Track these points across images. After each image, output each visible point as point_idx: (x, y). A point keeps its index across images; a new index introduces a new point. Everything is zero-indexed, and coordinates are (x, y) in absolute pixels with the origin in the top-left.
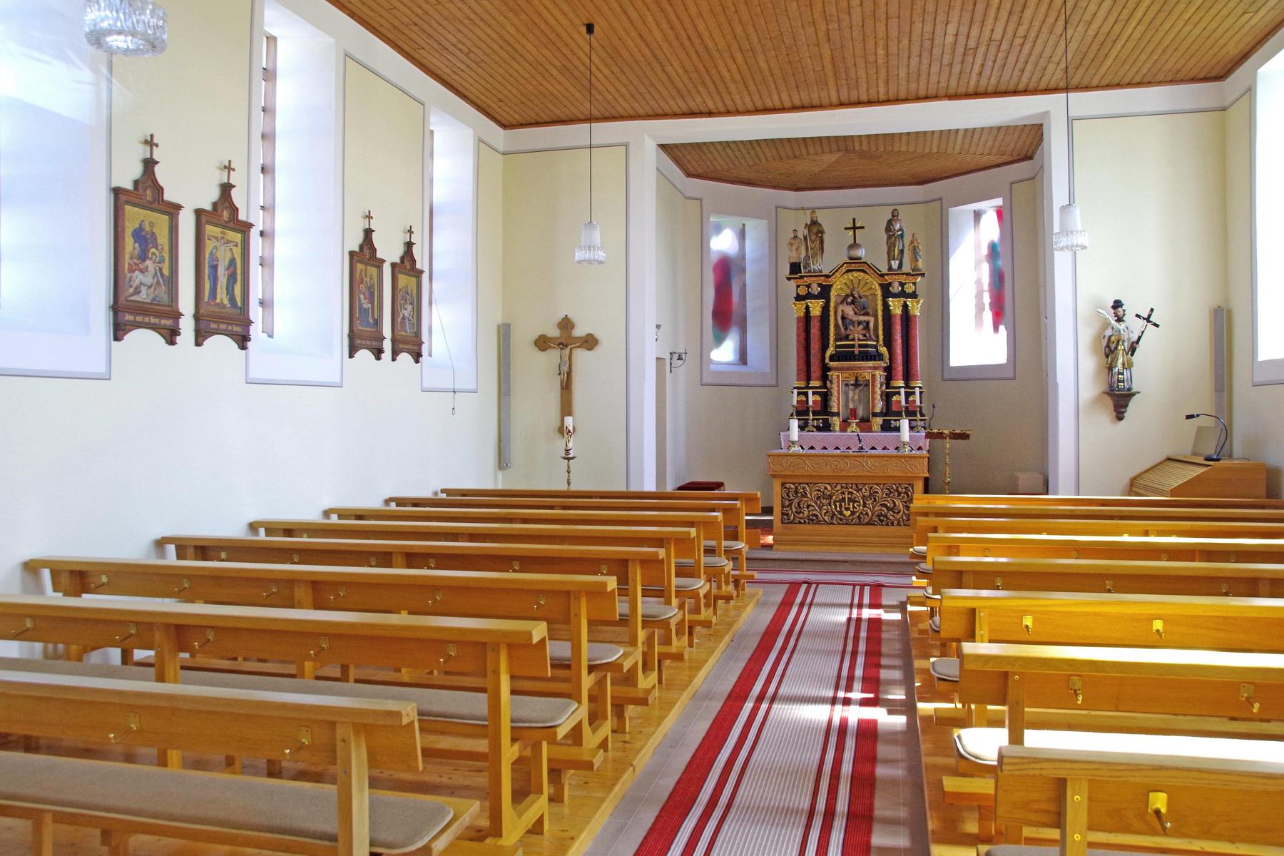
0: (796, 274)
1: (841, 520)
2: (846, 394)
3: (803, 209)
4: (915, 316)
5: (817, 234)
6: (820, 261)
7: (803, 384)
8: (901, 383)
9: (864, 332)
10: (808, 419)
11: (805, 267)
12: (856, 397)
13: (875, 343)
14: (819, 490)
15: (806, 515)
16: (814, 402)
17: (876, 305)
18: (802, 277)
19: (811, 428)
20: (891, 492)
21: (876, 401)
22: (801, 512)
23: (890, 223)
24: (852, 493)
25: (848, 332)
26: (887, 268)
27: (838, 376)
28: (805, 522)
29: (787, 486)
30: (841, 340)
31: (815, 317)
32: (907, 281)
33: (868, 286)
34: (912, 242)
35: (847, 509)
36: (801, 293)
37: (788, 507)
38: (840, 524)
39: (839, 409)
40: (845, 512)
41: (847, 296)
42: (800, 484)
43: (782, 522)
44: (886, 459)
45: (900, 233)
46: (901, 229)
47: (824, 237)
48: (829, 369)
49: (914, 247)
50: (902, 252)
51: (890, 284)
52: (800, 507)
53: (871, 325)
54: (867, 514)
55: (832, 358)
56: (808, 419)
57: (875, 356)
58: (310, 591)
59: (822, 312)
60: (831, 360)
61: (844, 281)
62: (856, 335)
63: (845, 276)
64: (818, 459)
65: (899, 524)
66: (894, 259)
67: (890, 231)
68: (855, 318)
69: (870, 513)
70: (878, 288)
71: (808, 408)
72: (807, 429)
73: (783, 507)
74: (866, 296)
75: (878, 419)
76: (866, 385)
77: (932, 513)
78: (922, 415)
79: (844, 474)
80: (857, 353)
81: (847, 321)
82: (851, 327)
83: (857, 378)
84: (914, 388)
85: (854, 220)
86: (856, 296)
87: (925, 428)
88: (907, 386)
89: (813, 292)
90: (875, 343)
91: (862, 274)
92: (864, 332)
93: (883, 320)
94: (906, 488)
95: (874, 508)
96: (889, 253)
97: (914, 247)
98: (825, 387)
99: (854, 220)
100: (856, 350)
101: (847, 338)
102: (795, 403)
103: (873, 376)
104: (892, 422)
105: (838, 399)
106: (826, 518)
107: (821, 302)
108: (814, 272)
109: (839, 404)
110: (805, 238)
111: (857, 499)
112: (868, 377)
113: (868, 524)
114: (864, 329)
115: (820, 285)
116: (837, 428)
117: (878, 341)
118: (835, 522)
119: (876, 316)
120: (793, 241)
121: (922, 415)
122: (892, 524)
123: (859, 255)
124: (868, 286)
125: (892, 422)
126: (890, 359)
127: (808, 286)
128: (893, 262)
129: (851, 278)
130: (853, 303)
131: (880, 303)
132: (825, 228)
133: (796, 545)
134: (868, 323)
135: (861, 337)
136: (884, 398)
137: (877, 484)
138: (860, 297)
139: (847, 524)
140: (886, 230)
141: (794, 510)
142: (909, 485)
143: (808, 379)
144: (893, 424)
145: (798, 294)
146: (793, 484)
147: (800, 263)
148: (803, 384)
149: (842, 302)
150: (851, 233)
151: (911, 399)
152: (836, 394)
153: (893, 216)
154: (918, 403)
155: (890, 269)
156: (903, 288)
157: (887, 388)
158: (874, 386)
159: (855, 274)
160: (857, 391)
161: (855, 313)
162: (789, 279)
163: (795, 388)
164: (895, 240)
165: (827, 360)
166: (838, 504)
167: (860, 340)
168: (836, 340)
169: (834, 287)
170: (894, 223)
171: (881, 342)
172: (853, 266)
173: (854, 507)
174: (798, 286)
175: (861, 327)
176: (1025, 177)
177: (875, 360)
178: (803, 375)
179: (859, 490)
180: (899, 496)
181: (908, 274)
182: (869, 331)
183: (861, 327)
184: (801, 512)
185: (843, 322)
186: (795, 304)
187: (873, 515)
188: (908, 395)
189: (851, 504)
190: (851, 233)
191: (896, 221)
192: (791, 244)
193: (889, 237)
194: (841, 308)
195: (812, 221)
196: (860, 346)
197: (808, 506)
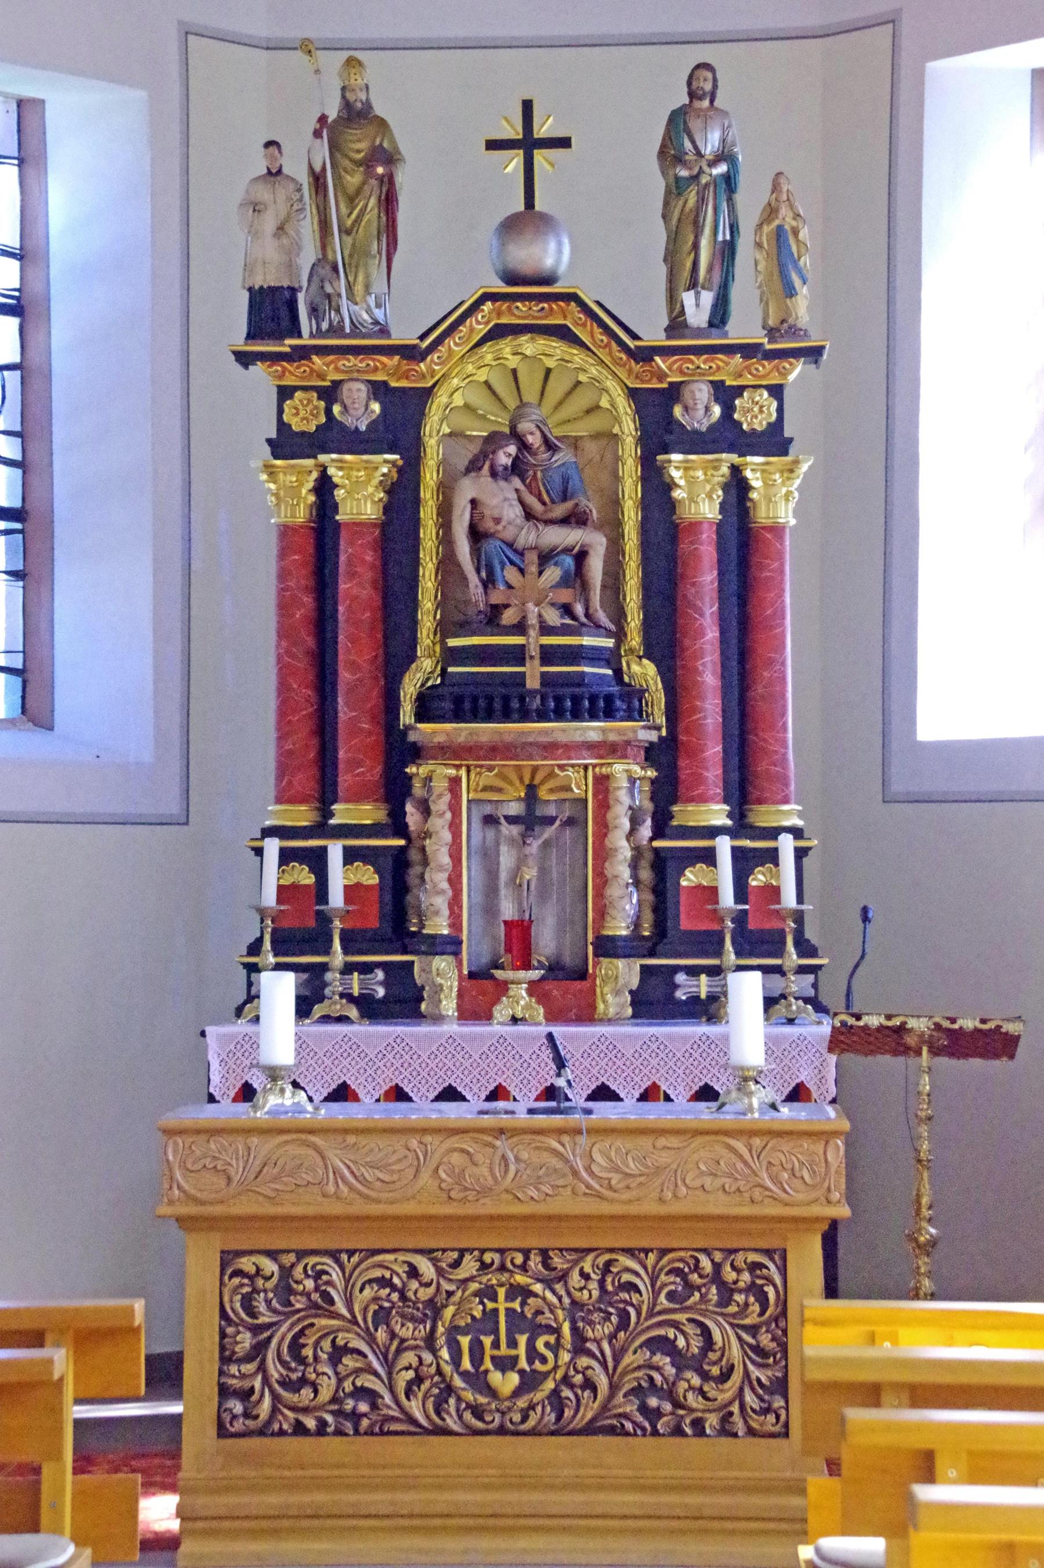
0: (279, 336)
1: (478, 1412)
2: (489, 858)
3: (307, 47)
4: (777, 530)
5: (367, 164)
6: (379, 285)
7: (302, 815)
8: (718, 814)
9: (565, 596)
10: (324, 967)
11: (314, 311)
12: (530, 873)
13: (610, 643)
14: (383, 1282)
15: (325, 1395)
16: (351, 892)
17: (617, 478)
18: (302, 354)
19: (338, 1007)
20: (690, 1287)
21: (614, 891)
22: (303, 1381)
23: (678, 121)
24: (526, 1293)
25: (497, 597)
26: (665, 322)
27: (455, 781)
28: (322, 1424)
29: (246, 1264)
30: (464, 627)
31: (358, 527)
32: (748, 380)
33: (581, 401)
34: (771, 212)
35: (505, 1364)
36: (297, 425)
37: (248, 1359)
38: (477, 1432)
39: (456, 923)
40: (495, 1378)
41: (493, 440)
42: (301, 1254)
43: (222, 1432)
44: (674, 1141)
45: (722, 169)
46: (724, 155)
47: (400, 178)
48: (416, 753)
49: (780, 231)
50: (727, 252)
51: (674, 393)
52: (302, 1361)
53: (596, 567)
54: (590, 1385)
55: (425, 711)
56: (324, 967)
57: (609, 699)
58: (515, 622)
59: (387, 509)
60: (425, 711)
61: (482, 376)
62: (532, 610)
63: (487, 352)
64: (382, 1142)
65: (726, 1430)
66: (693, 284)
67: (679, 159)
68: (528, 536)
69: (603, 1382)
70: (624, 406)
71: (324, 919)
72: (318, 1010)
73: (226, 1358)
74: (575, 443)
75: (620, 963)
76: (570, 822)
77: (898, 1387)
78: (805, 948)
79: (488, 1207)
80: (533, 683)
81: (491, 546)
82: (511, 574)
83: (532, 790)
84: (774, 833)
85: (527, 107)
86: (534, 440)
87: (820, 1008)
88: (741, 826)
89: (349, 421)
90: (610, 643)
91: (558, 347)
92: (565, 596)
93: (645, 545)
94: (754, 1267)
95: (617, 1358)
96: (671, 257)
97: (780, 231)
98: (399, 827)
99: (527, 107)
100: (533, 673)
101: (492, 618)
102: (270, 898)
103: (603, 783)
104: (681, 978)
105: (454, 881)
106: (415, 1408)
107: (385, 463)
108: (356, 332)
109: (455, 903)
110: (318, 180)
111: (546, 1319)
112: (580, 786)
113: (589, 1430)
114: (565, 582)
115: (379, 390)
116: (449, 1006)
117: (620, 635)
118: (452, 1423)
119: (614, 528)
120: (263, 193)
121: (805, 948)
122: (698, 1426)
123: (549, 262)
124: (581, 401)
125: (681, 978)
126: (672, 712)
127: (330, 394)
128: (688, 298)
129: (513, 362)
130: (517, 468)
131: (630, 470)
132: (404, 139)
133: (275, 1533)
134: (581, 556)
135: (553, 617)
136: (646, 874)
137: (629, 1252)
138: (550, 446)
139: (502, 1431)
140: (662, 153)
141: (275, 1371)
142: (768, 1253)
143: (326, 797)
144: (685, 987)
145: (282, 426)
146: (272, 1254)
147: (293, 291)
148: (302, 815)
149: (473, 467)
150: (514, 162)
151: (758, 879)
152: (446, 860)
153: (692, 95)
154: (789, 899)
155: (677, 325)
156: (728, 409)
157: (659, 832)
158: (603, 828)
159: (530, 346)
160: (534, 846)
161: (529, 515)
162: (244, 359)
163: (268, 832)
164: (702, 200)
165: (407, 715)
166: (465, 1341)
167: (546, 630)
168: (445, 629)
169: (441, 398)
170: (695, 125)
171: (635, 639)
172: (521, 313)
173: (532, 1354)
174: (285, 393)
175: (553, 574)
176: (61, 806)
177: (609, 714)
178: (306, 780)
179: (555, 1278)
180: (725, 1300)
181: (749, 351)
182: (585, 587)
183: (553, 574)
184: (303, 1381)
185: (476, 552)
186: (271, 472)
187: (613, 1388)
188: (744, 861)
189: (522, 1340)
190: (514, 162)
191: (705, 117)
192: (257, 208)
193: (676, 189)
194: (467, 489)
195: (347, 105)
196: (548, 655)
197: (338, 1353)
